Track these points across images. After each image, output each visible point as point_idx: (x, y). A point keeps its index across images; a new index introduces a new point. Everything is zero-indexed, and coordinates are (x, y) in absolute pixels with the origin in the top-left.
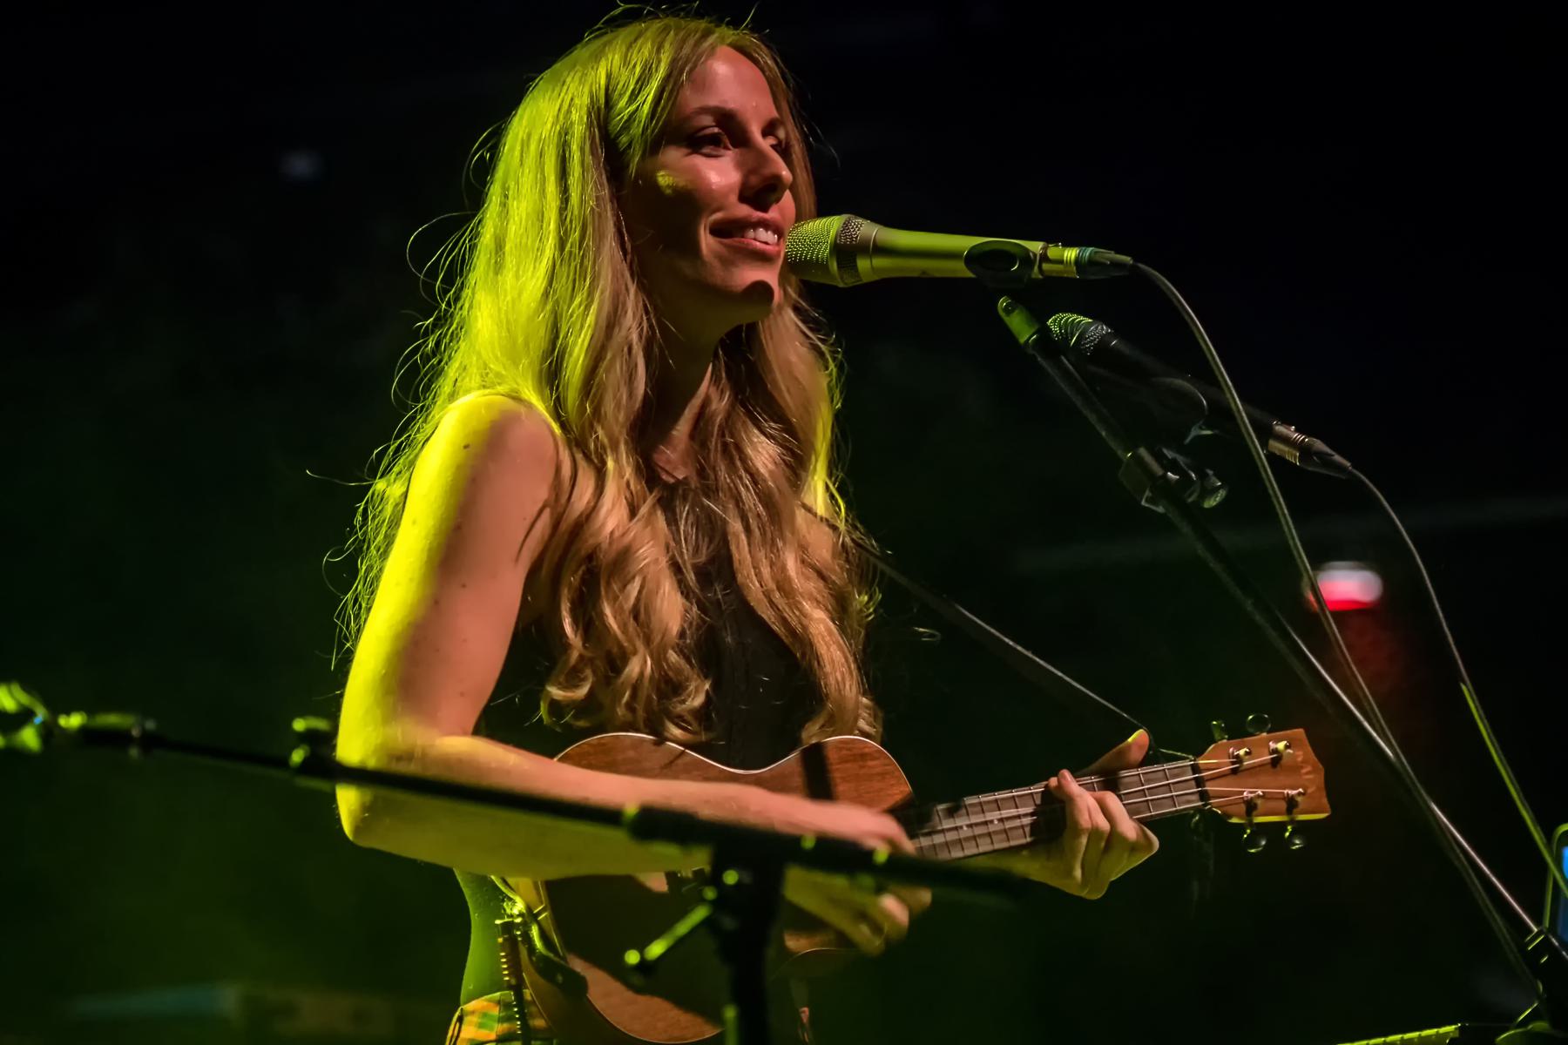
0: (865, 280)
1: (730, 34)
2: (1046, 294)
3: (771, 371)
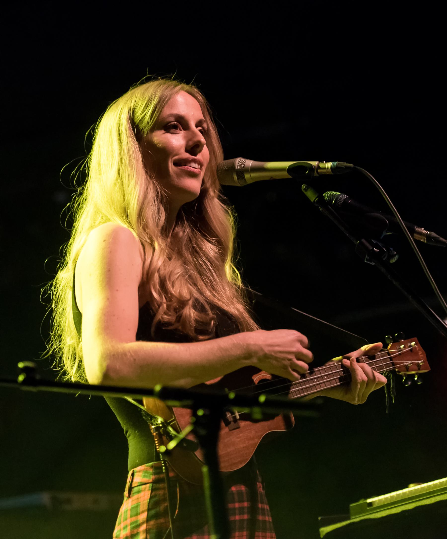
0: (249, 182)
1: (187, 87)
2: (323, 182)
3: (212, 222)
